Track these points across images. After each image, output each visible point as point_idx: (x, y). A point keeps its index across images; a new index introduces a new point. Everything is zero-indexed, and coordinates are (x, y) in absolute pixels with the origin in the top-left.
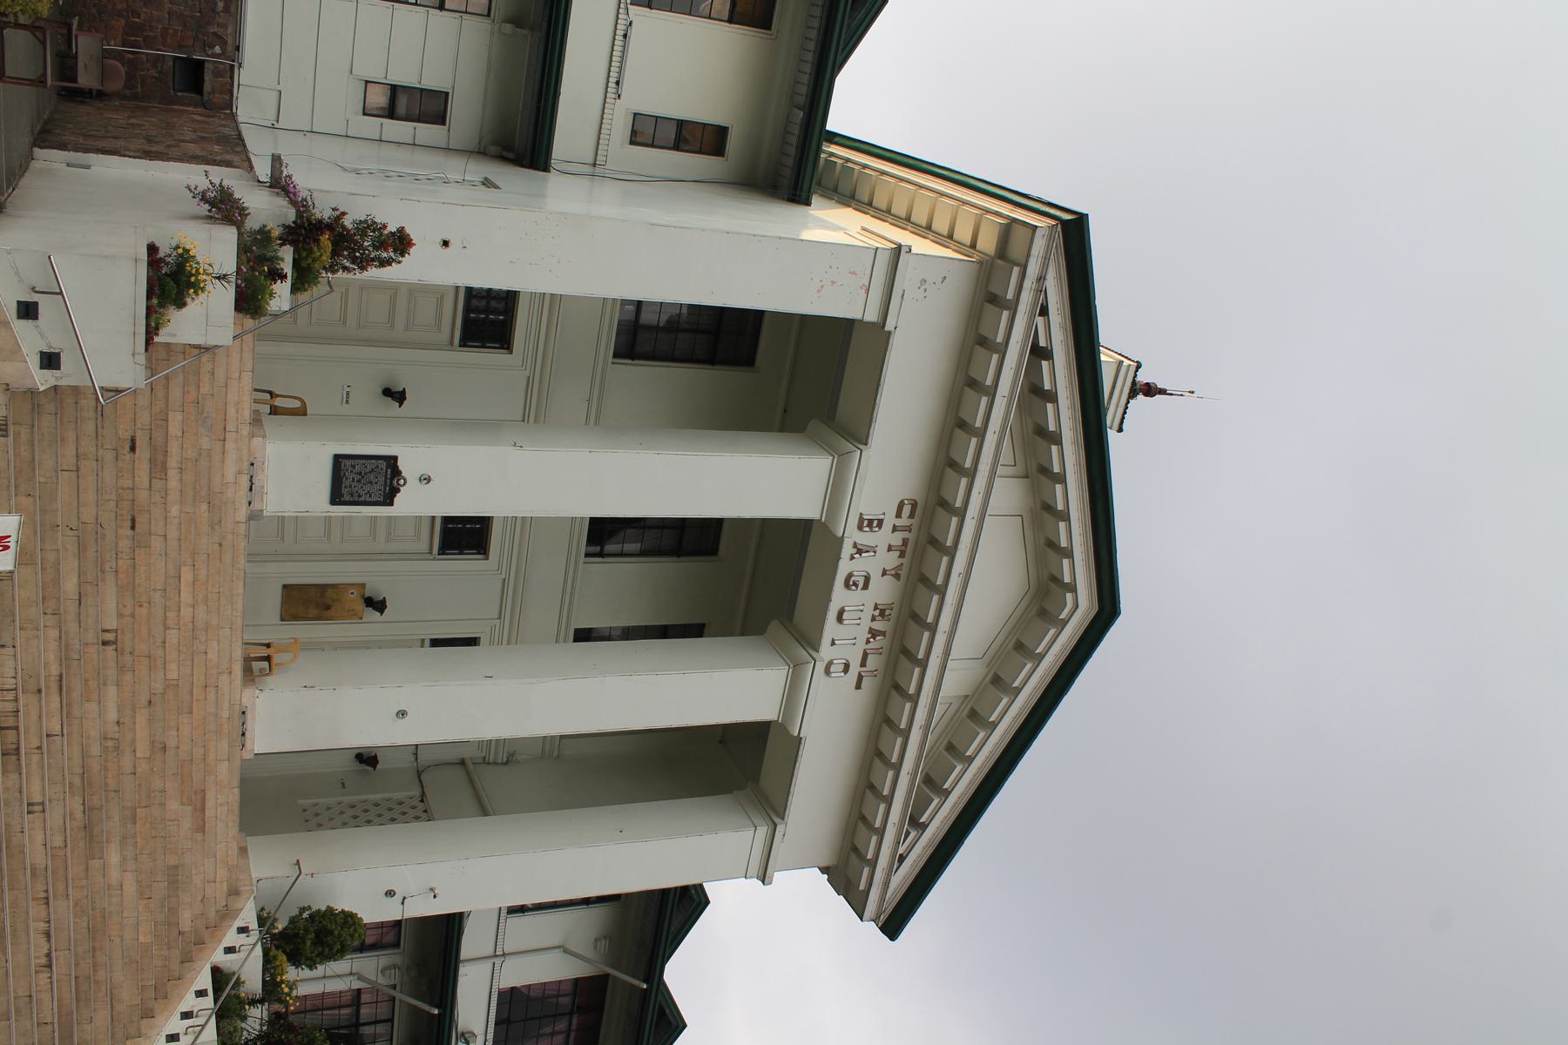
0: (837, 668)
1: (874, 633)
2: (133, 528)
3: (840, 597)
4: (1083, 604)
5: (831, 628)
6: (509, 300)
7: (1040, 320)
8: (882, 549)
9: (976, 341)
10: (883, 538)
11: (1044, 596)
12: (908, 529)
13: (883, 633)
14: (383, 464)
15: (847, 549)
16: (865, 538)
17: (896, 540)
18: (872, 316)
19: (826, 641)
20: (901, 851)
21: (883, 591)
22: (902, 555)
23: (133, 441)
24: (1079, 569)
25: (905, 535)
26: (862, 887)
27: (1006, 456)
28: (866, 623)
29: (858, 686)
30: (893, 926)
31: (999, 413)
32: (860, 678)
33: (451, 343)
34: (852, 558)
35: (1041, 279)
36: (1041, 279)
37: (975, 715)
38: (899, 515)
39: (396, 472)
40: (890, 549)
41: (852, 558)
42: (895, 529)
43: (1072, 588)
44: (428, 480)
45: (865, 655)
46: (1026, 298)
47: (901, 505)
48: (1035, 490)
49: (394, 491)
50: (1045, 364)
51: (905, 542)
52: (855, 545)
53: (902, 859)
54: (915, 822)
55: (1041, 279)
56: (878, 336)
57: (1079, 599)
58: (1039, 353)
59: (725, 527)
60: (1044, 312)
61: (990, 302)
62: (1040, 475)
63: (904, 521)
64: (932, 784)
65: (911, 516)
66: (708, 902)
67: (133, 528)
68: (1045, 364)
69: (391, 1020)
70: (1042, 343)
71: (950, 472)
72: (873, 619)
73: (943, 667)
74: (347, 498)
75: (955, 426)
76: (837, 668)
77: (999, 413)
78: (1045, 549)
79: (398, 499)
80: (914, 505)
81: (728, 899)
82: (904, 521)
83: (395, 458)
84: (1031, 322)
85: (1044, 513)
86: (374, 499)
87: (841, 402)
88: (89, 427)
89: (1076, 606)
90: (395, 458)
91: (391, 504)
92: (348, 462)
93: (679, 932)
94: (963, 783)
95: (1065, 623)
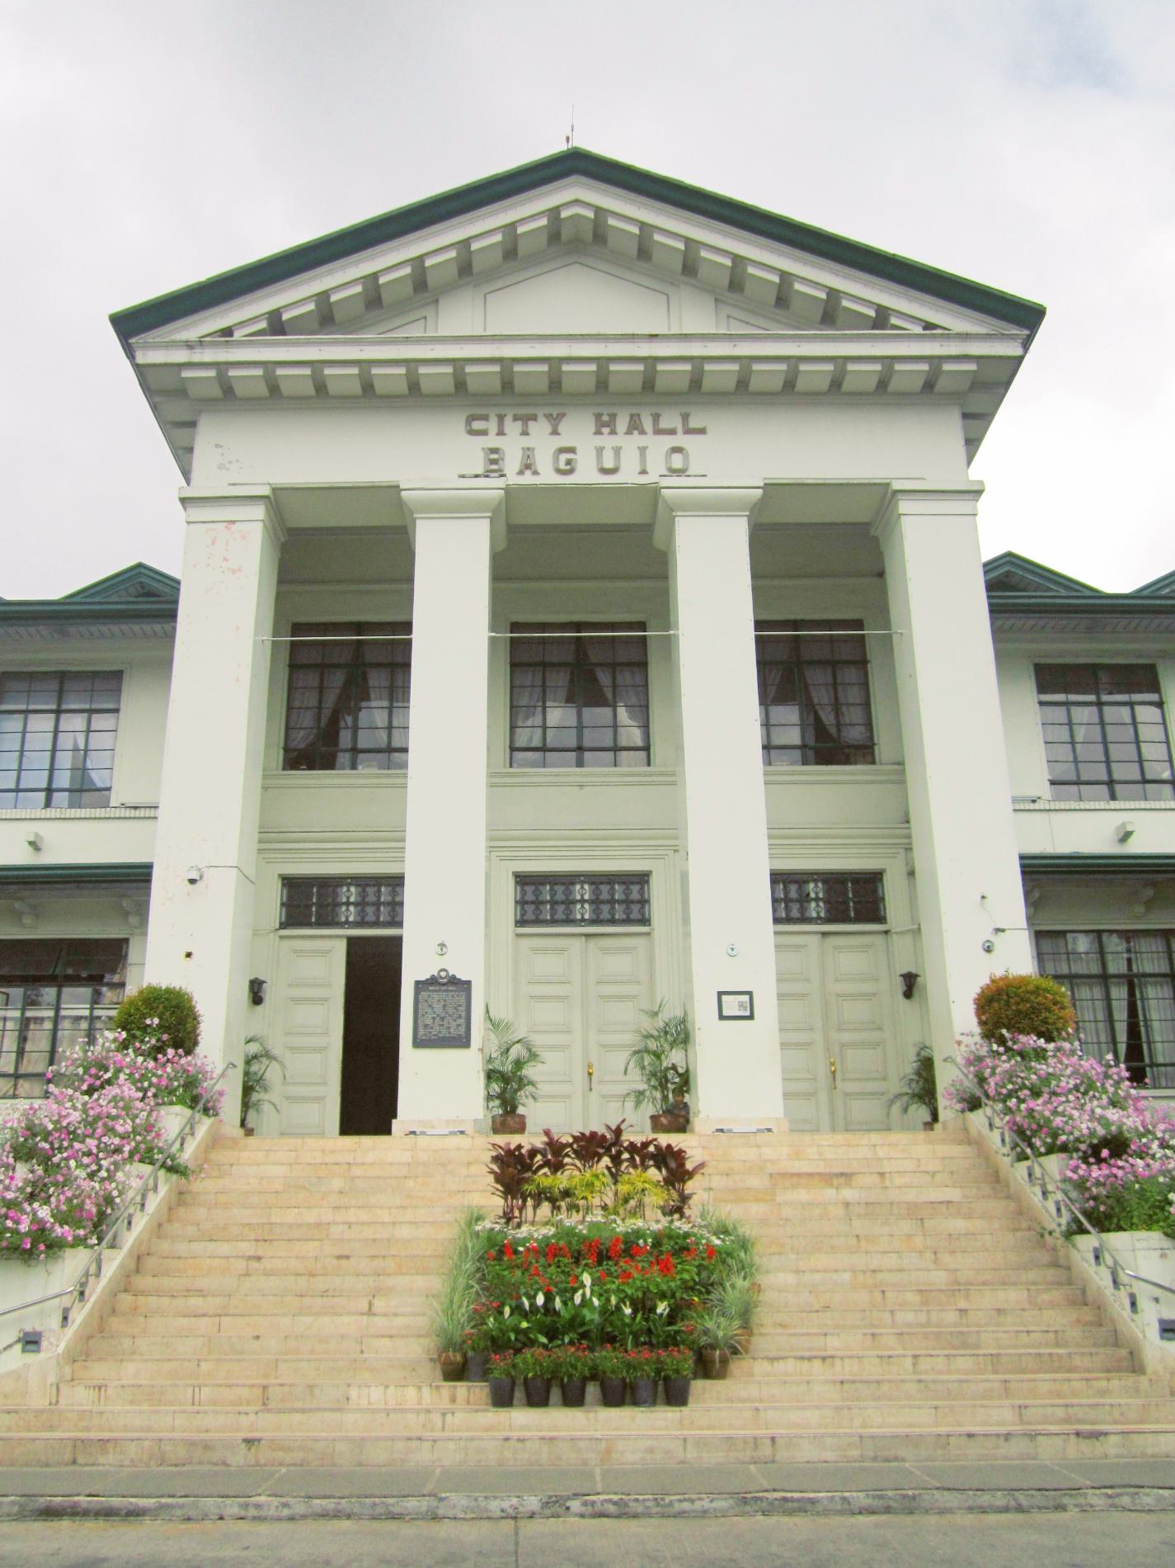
0: (677, 461)
1: (635, 426)
2: (347, 1257)
3: (586, 474)
4: (576, 197)
5: (628, 475)
6: (778, 878)
7: (238, 335)
8: (526, 442)
9: (273, 396)
10: (512, 445)
11: (575, 244)
12: (501, 418)
13: (685, 418)
14: (424, 994)
15: (528, 479)
16: (512, 465)
17: (513, 428)
18: (259, 512)
19: (643, 479)
20: (918, 330)
21: (578, 431)
22: (534, 418)
23: (339, 1257)
24: (527, 212)
25: (508, 421)
26: (972, 367)
27: (416, 331)
28: (621, 439)
29: (702, 431)
30: (1024, 317)
31: (379, 349)
32: (688, 431)
33: (648, 934)
34: (536, 473)
35: (189, 345)
36: (189, 345)
37: (736, 283)
38: (484, 433)
39: (433, 981)
40: (525, 433)
41: (536, 473)
42: (501, 433)
43: (554, 213)
44: (442, 945)
45: (658, 432)
46: (208, 356)
47: (472, 432)
48: (449, 288)
49: (454, 981)
50: (286, 316)
51: (516, 418)
52: (521, 473)
53: (929, 326)
54: (881, 319)
55: (188, 348)
56: (278, 502)
57: (579, 204)
58: (277, 326)
59: (761, 618)
60: (228, 332)
61: (652, 387)
62: (423, 288)
63: (492, 425)
64: (830, 314)
65: (485, 418)
66: (1009, 554)
67: (347, 1257)
68: (286, 316)
69: (1099, 933)
70: (263, 325)
71: (893, 386)
72: (613, 432)
73: (632, 338)
74: (462, 1030)
75: (368, 396)
76: (677, 461)
77: (379, 349)
78: (514, 257)
79: (462, 976)
80: (471, 418)
81: (1000, 532)
82: (492, 425)
83: (417, 983)
84: (240, 344)
85: (467, 270)
86: (462, 1000)
87: (376, 522)
88: (166, 1301)
89: (577, 202)
90: (417, 983)
91: (469, 983)
92: (421, 1031)
93: (1066, 587)
94: (816, 277)
95: (598, 210)
